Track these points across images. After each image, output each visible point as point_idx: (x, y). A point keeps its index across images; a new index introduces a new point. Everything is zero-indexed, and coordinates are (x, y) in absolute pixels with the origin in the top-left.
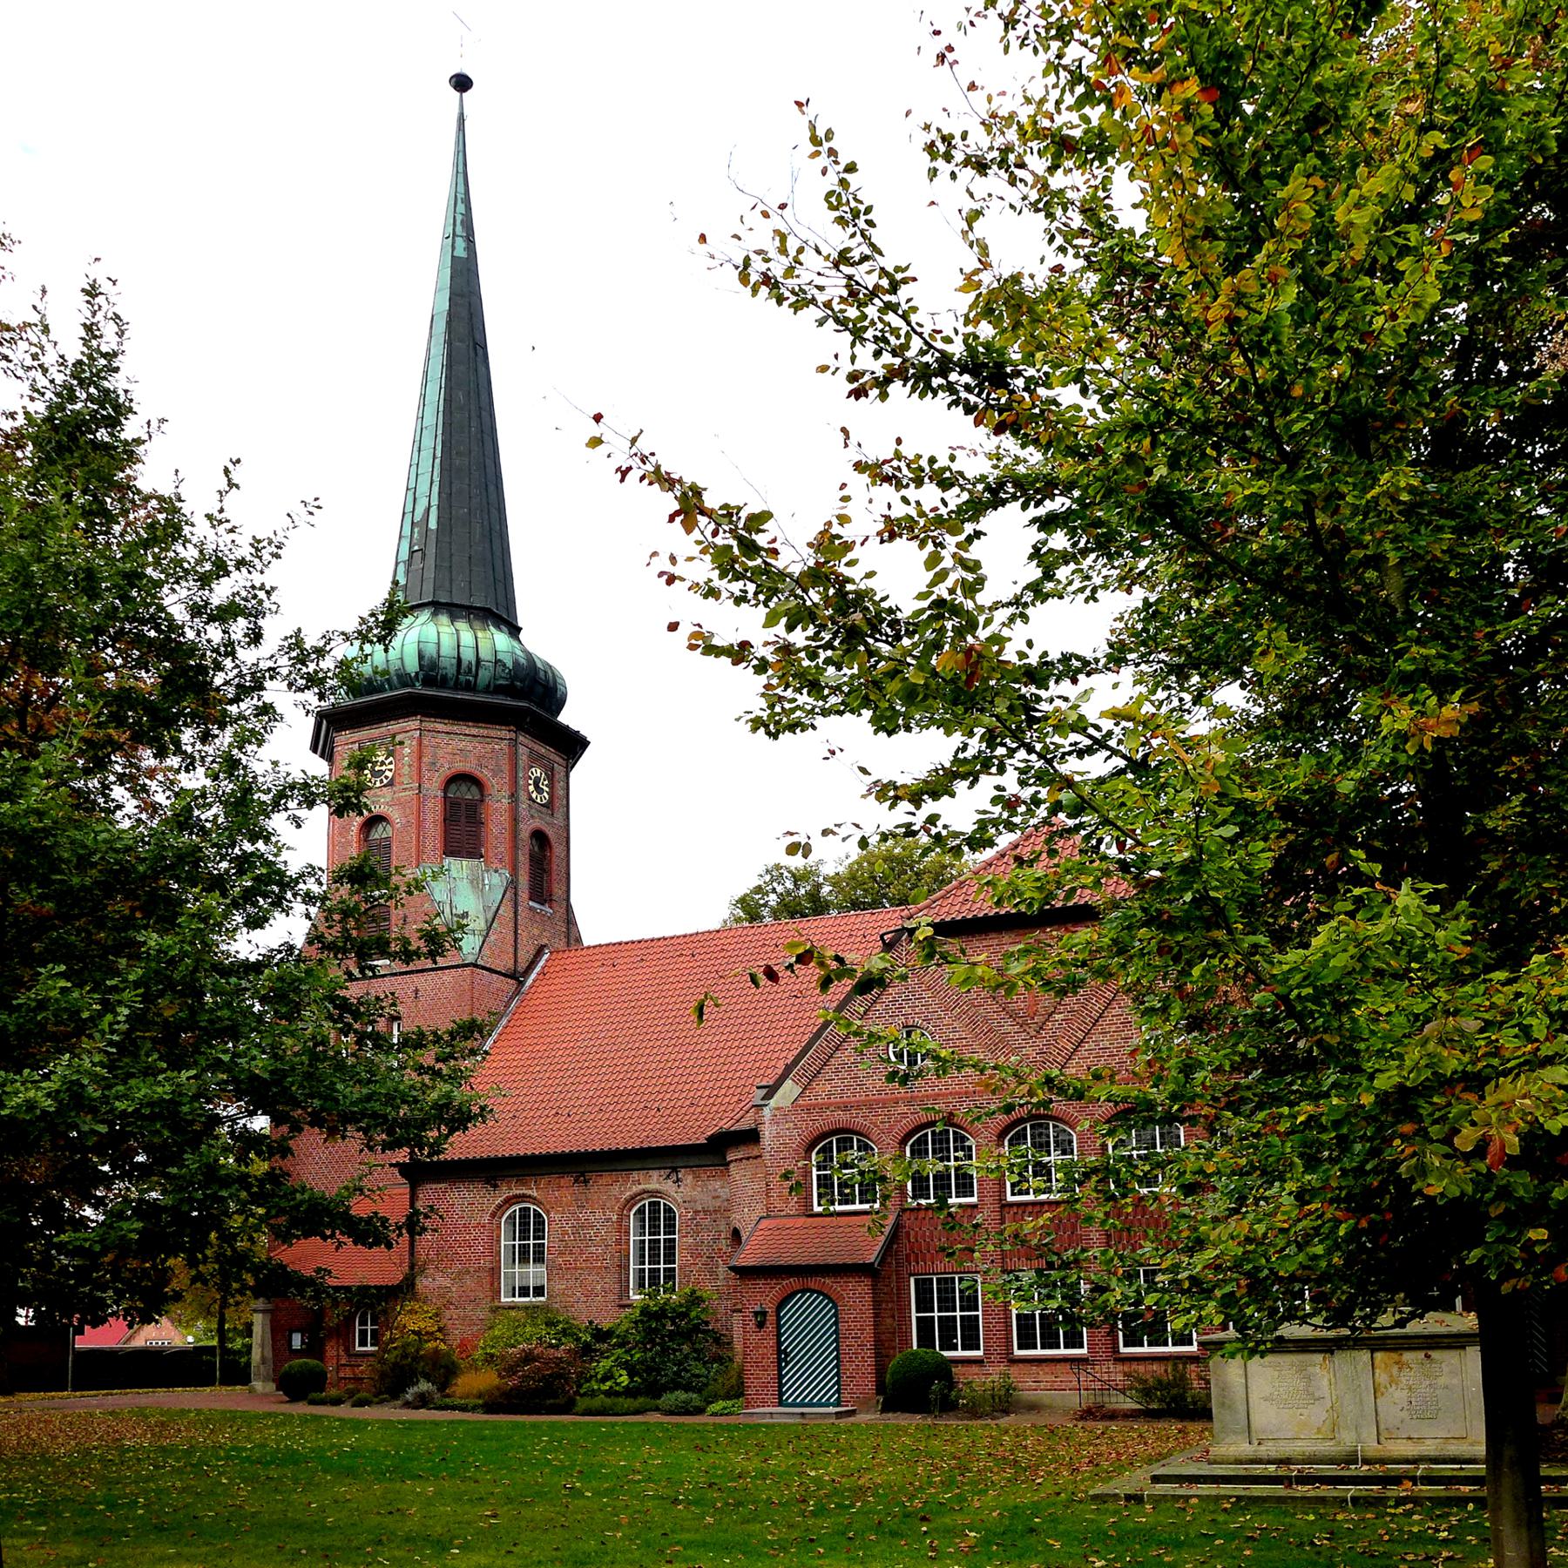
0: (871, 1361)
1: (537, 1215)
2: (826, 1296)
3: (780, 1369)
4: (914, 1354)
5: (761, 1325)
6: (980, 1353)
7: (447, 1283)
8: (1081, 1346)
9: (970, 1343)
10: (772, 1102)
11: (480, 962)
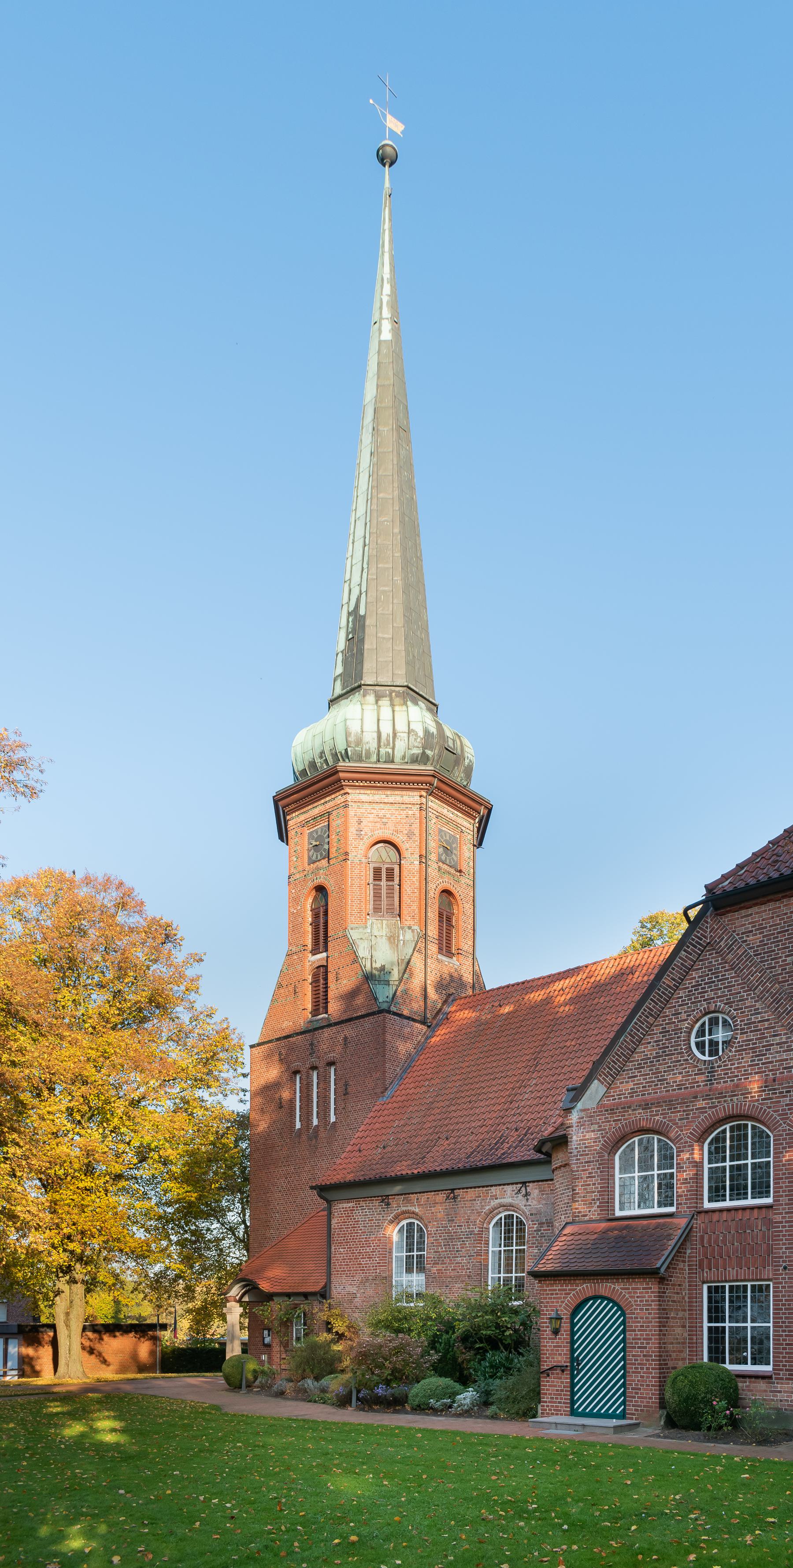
0: (655, 1373)
2: (615, 1304)
3: (573, 1377)
5: (556, 1332)
6: (769, 1368)
7: (354, 1290)
9: (760, 1358)
10: (580, 1105)
11: (393, 1009)
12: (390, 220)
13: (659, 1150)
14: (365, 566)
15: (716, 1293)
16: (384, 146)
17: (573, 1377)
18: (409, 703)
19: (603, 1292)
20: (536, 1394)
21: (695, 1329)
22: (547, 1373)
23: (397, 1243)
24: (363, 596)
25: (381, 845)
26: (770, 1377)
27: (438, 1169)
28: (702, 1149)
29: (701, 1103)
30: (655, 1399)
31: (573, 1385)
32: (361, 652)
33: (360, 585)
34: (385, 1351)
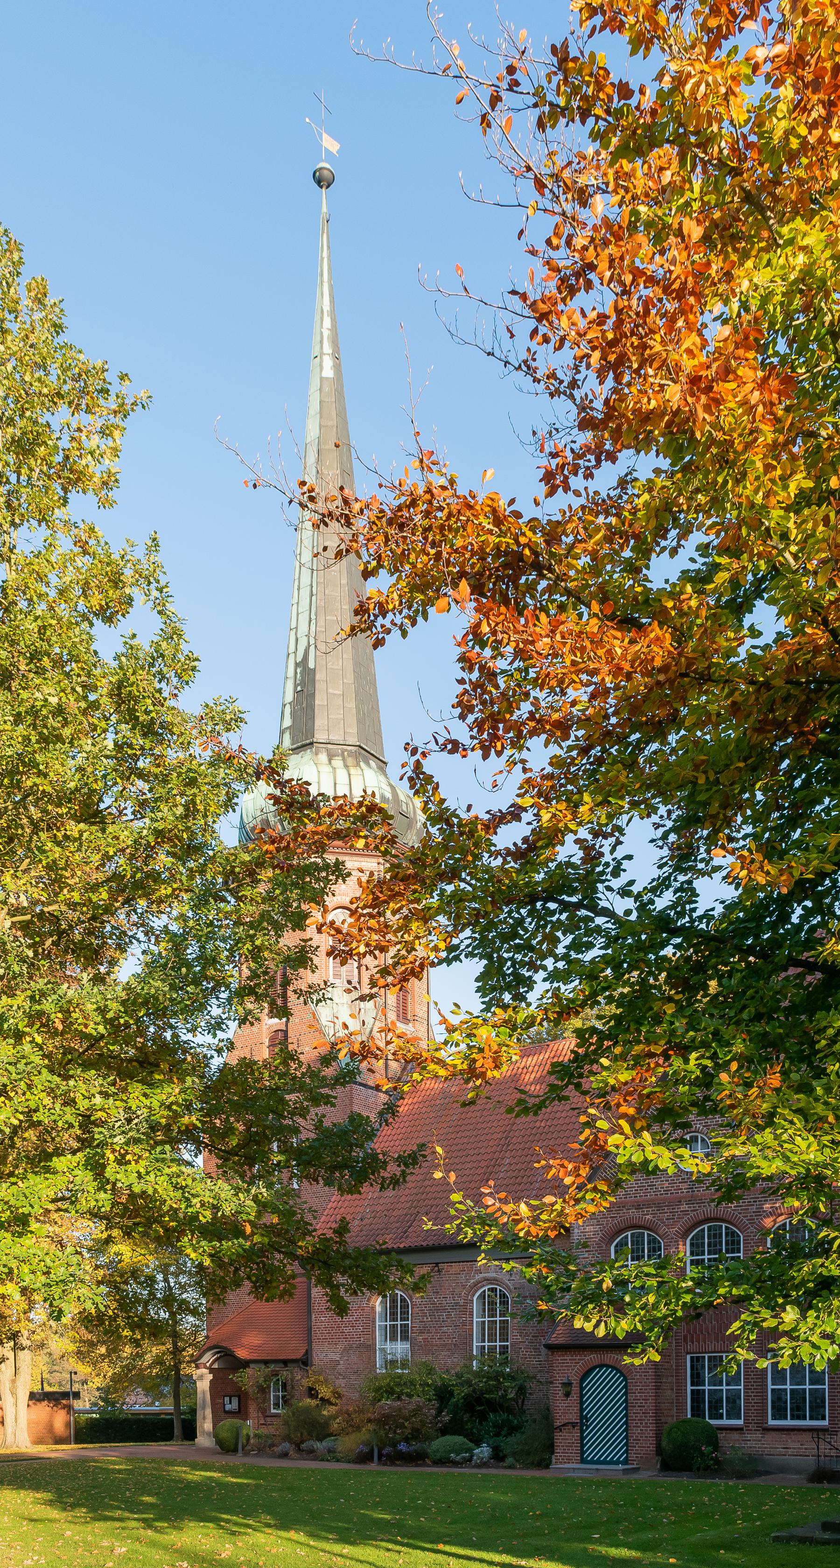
0: (652, 1427)
1: (403, 1300)
3: (582, 1432)
4: (690, 1421)
5: (567, 1395)
6: (740, 1422)
7: (337, 1357)
8: (824, 1418)
9: (734, 1413)
12: (329, 247)
13: (649, 1243)
14: (313, 617)
15: (697, 1362)
16: (321, 169)
17: (582, 1432)
18: (362, 764)
19: (608, 1362)
20: (551, 1448)
21: (681, 1391)
22: (560, 1429)
23: (380, 1314)
24: (312, 648)
25: (340, 910)
26: (742, 1429)
27: (424, 1244)
28: (685, 1244)
29: (684, 1207)
30: (653, 1448)
31: (582, 1438)
32: (311, 708)
33: (308, 636)
34: (405, 1412)
